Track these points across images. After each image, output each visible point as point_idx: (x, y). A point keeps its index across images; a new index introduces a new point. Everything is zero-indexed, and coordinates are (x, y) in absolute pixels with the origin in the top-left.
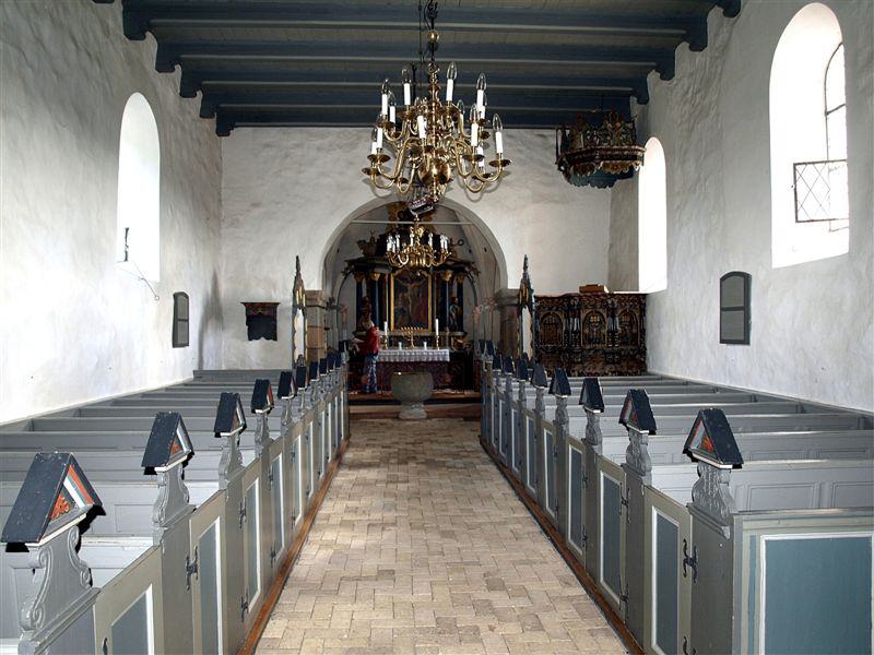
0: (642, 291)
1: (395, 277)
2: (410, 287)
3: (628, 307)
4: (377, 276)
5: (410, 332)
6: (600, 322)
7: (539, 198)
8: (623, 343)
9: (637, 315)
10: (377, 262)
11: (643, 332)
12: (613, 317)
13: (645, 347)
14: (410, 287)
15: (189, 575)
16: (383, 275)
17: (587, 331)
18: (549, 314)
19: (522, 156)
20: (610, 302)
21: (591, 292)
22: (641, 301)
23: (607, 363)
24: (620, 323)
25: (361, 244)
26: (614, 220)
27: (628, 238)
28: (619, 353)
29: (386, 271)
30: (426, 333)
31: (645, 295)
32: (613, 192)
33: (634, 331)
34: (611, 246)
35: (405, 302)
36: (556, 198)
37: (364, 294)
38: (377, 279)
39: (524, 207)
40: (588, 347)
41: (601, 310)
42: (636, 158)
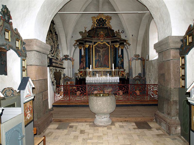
2: (101, 50)
14: (101, 50)
25: (81, 33)
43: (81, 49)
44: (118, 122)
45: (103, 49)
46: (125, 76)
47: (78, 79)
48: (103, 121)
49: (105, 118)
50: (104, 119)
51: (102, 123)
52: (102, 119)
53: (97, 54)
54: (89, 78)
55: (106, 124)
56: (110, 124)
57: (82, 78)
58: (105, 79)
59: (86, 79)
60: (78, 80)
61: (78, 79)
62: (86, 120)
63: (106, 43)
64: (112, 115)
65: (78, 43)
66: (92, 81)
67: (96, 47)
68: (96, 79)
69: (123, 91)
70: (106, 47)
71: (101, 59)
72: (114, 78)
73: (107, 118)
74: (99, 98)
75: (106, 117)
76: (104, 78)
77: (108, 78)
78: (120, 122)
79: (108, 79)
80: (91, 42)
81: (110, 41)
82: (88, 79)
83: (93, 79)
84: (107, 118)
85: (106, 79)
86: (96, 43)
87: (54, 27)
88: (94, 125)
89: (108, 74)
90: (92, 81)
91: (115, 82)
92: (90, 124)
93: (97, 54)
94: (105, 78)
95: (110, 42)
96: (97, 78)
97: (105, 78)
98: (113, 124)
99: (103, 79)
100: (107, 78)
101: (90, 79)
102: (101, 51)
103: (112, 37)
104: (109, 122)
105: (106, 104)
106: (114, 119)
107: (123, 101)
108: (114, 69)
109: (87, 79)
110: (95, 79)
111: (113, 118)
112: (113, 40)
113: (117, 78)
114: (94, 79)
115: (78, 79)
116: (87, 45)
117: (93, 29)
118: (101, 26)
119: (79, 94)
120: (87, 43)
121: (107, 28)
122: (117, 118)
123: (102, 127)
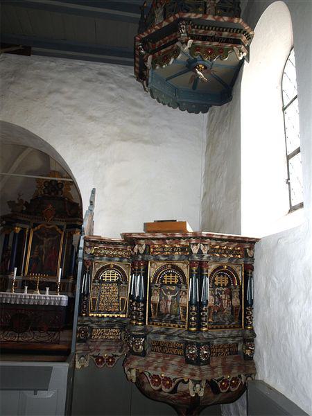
0: (246, 232)
1: (34, 232)
2: (45, 240)
3: (226, 261)
4: (18, 230)
5: (38, 278)
6: (178, 285)
7: (125, 137)
8: (217, 325)
9: (241, 274)
10: (19, 218)
11: (249, 304)
12: (200, 277)
13: (252, 330)
14: (45, 240)
15: (34, 390)
16: (23, 230)
17: (156, 298)
18: (108, 267)
19: (113, 94)
20: (195, 250)
21: (167, 230)
22: (245, 248)
23: (188, 362)
24: (213, 286)
25: (11, 204)
26: (208, 165)
27: (225, 175)
28: (208, 343)
29: (27, 227)
30: (51, 280)
31: (252, 242)
32: (210, 120)
33: (235, 302)
34: (205, 194)
35: (40, 253)
36: (146, 139)
37: (10, 244)
38: (18, 232)
39: (109, 144)
40: (156, 328)
41: (180, 265)
42: (238, 39)
43: (9, 235)
45: (49, 239)
53: (37, 247)
63: (57, 227)
65: (4, 222)
66: (11, 301)
67: (36, 233)
70: (54, 236)
71: (44, 257)
80: (26, 223)
81: (64, 224)
86: (37, 225)
87: (17, 202)
89: (48, 289)
90: (11, 301)
91: (52, 304)
93: (37, 247)
95: (65, 227)
96: (46, 297)
102: (45, 242)
103: (69, 217)
108: (17, 275)
112: (69, 223)
116: (18, 227)
117: (35, 199)
118: (53, 194)
120: (17, 224)
121: (63, 199)
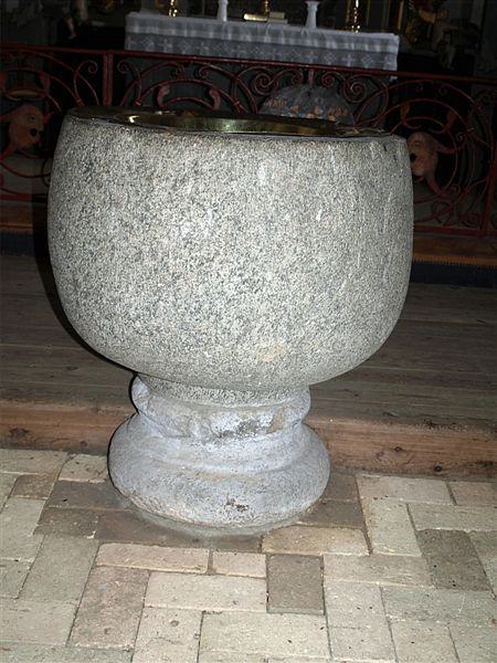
44: (403, 472)
46: (443, 43)
47: (71, 26)
48: (225, 470)
49: (248, 428)
50: (234, 447)
51: (200, 495)
52: (211, 446)
54: (154, 23)
55: (258, 513)
56: (306, 504)
57: (101, 24)
58: (283, 41)
59: (129, 29)
60: (74, 36)
61: (71, 26)
62: (22, 422)
64: (332, 397)
68: (211, 35)
69: (445, 140)
72: (357, 41)
73: (273, 427)
74: (188, 159)
75: (265, 419)
76: (275, 34)
77: (314, 36)
78: (422, 473)
79: (308, 43)
82: (143, 24)
83: (185, 33)
84: (273, 427)
85: (292, 42)
88: (109, 515)
92: (61, 486)
94: (287, 35)
96: (218, 29)
97: (287, 35)
98: (338, 506)
99: (267, 39)
100: (298, 35)
101: (156, 30)
104: (293, 491)
105: (291, 257)
106: (361, 435)
107: (432, 229)
109: (137, 29)
110: (200, 28)
111: (351, 424)
113: (385, 43)
114: (194, 34)
115: (69, 33)
119: (33, 132)
122: (396, 429)
123: (202, 554)
